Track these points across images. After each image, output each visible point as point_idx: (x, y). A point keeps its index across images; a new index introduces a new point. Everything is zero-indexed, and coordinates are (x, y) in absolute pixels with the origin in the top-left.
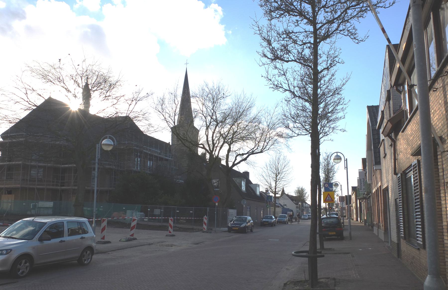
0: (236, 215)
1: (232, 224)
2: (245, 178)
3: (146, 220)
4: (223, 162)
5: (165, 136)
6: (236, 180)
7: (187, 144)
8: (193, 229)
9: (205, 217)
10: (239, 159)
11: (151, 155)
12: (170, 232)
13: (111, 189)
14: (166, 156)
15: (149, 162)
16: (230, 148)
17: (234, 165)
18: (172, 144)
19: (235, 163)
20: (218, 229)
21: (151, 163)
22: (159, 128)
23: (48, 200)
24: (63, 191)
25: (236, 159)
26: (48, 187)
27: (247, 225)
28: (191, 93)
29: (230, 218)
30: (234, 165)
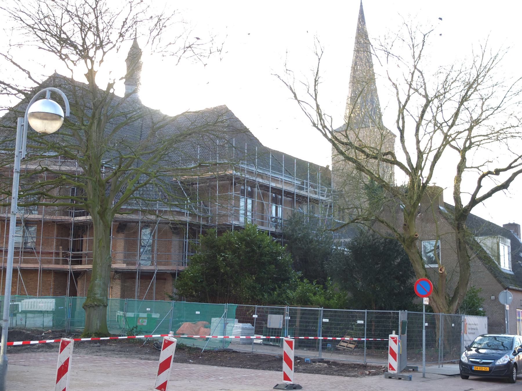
0: (485, 331)
1: (472, 356)
2: (509, 238)
3: (259, 341)
4: (449, 199)
5: (320, 154)
6: (486, 243)
7: (352, 154)
8: (365, 367)
9: (393, 335)
10: (488, 184)
11: (278, 191)
12: (286, 378)
13: (181, 268)
14: (316, 193)
15: (274, 208)
16: (464, 159)
17: (474, 202)
18: (333, 168)
19: (478, 196)
20: (434, 367)
21: (280, 210)
22: (295, 132)
23: (43, 294)
24: (78, 274)
25: (479, 187)
26: (46, 266)
27: (515, 359)
28: (424, 118)
29: (467, 338)
30: (474, 202)
